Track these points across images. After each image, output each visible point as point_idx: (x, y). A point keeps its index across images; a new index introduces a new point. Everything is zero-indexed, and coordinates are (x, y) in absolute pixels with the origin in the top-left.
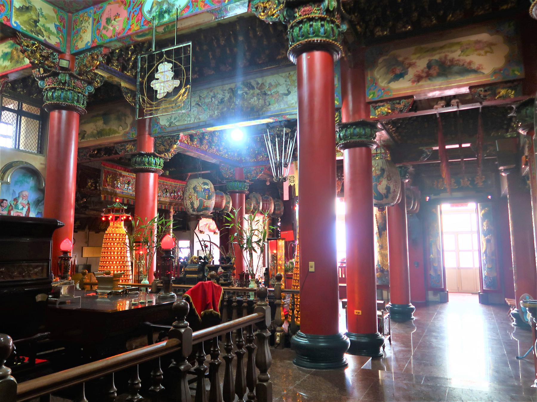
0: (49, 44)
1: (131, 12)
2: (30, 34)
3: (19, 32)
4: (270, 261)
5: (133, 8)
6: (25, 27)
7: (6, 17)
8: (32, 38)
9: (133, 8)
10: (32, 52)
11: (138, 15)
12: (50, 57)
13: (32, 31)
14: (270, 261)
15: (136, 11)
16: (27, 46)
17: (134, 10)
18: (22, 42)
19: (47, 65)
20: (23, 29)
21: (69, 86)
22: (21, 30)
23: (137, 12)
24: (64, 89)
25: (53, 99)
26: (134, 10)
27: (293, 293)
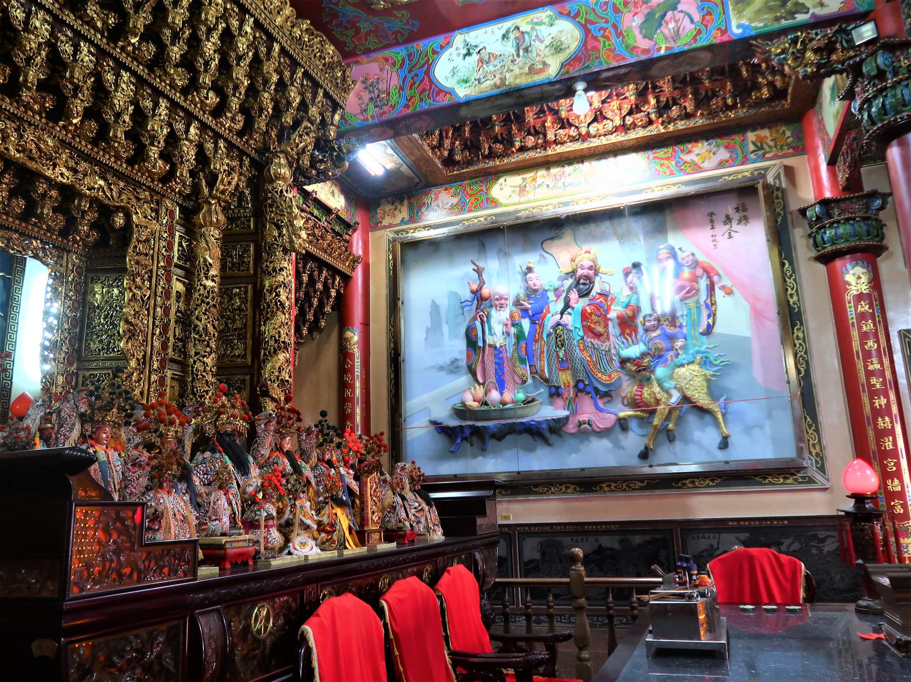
0: (826, 16)
1: (406, 77)
2: (775, 26)
3: (755, 38)
4: (235, 545)
5: (410, 71)
6: (760, 21)
7: (719, 29)
8: (784, 32)
9: (410, 71)
10: (795, 59)
11: (421, 82)
12: (835, 42)
13: (777, 19)
14: (235, 545)
15: (417, 75)
16: (783, 52)
17: (413, 73)
18: (770, 51)
19: (838, 62)
20: (756, 28)
21: (895, 74)
22: (753, 33)
23: (420, 78)
24: (885, 89)
25: (886, 114)
26: (413, 73)
27: (332, 124)
